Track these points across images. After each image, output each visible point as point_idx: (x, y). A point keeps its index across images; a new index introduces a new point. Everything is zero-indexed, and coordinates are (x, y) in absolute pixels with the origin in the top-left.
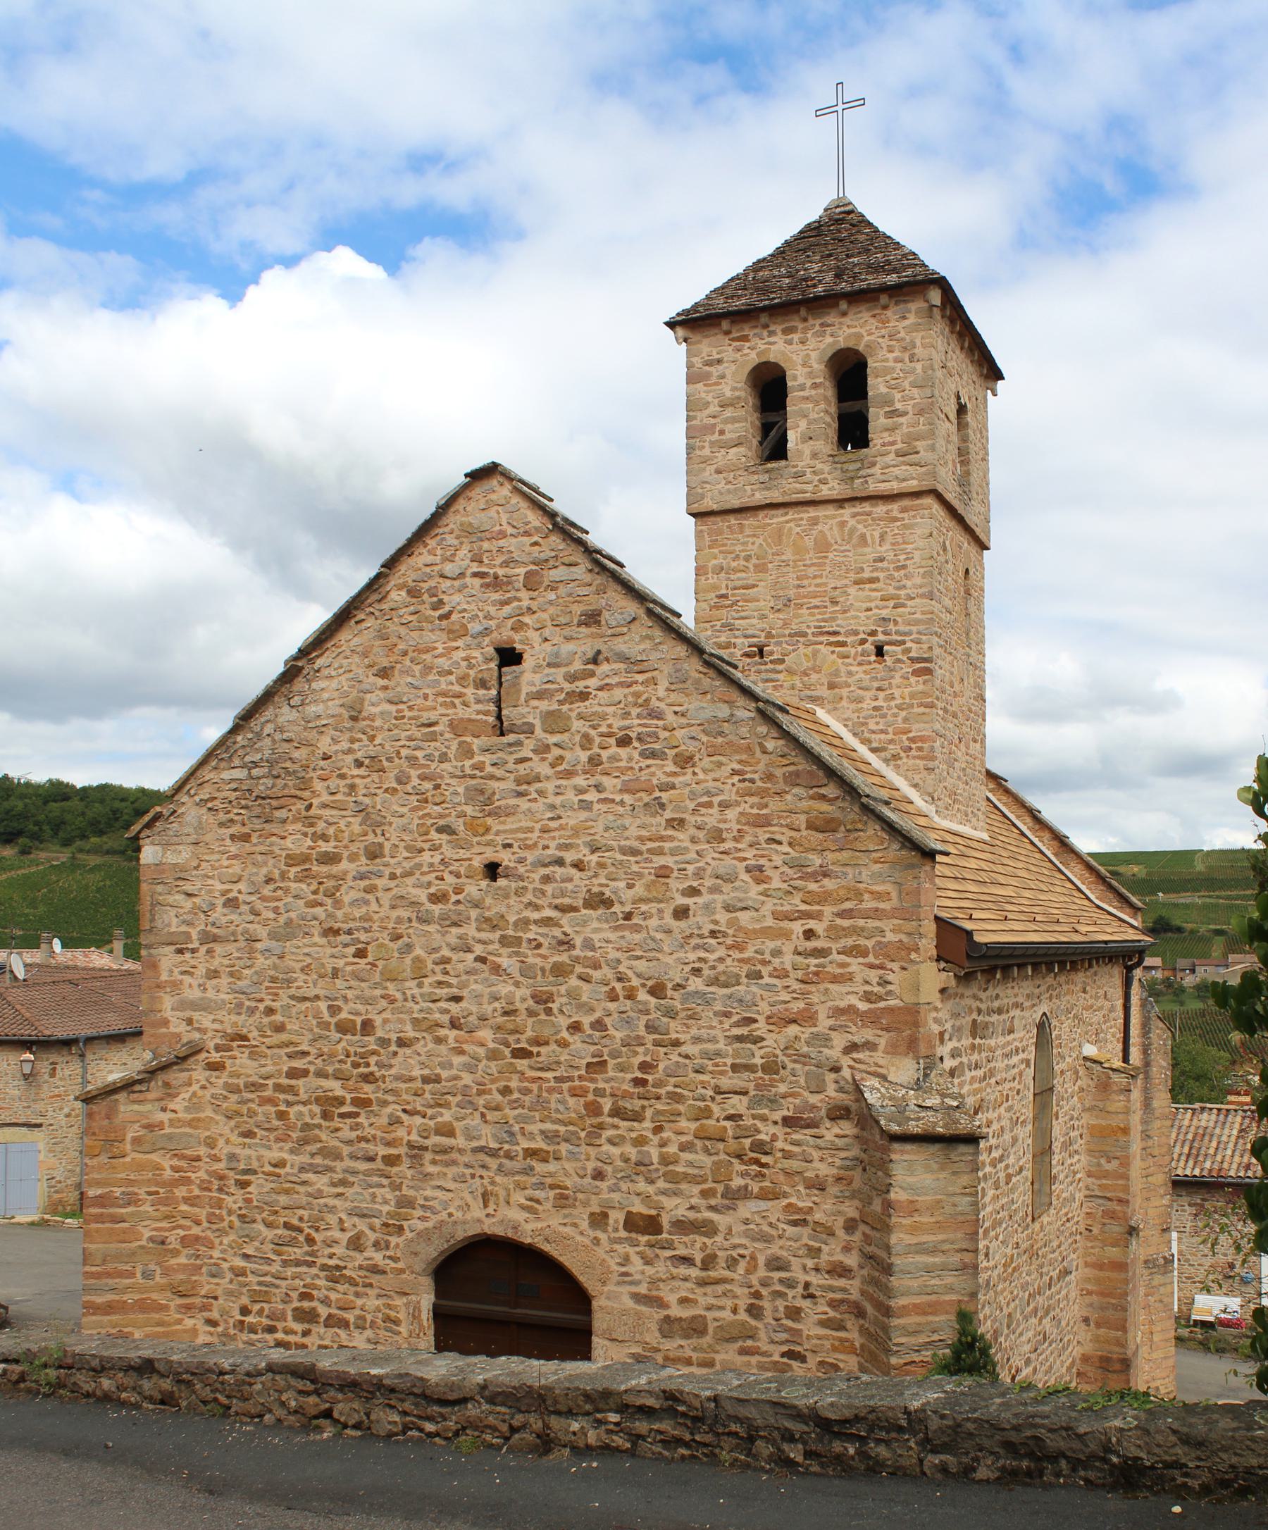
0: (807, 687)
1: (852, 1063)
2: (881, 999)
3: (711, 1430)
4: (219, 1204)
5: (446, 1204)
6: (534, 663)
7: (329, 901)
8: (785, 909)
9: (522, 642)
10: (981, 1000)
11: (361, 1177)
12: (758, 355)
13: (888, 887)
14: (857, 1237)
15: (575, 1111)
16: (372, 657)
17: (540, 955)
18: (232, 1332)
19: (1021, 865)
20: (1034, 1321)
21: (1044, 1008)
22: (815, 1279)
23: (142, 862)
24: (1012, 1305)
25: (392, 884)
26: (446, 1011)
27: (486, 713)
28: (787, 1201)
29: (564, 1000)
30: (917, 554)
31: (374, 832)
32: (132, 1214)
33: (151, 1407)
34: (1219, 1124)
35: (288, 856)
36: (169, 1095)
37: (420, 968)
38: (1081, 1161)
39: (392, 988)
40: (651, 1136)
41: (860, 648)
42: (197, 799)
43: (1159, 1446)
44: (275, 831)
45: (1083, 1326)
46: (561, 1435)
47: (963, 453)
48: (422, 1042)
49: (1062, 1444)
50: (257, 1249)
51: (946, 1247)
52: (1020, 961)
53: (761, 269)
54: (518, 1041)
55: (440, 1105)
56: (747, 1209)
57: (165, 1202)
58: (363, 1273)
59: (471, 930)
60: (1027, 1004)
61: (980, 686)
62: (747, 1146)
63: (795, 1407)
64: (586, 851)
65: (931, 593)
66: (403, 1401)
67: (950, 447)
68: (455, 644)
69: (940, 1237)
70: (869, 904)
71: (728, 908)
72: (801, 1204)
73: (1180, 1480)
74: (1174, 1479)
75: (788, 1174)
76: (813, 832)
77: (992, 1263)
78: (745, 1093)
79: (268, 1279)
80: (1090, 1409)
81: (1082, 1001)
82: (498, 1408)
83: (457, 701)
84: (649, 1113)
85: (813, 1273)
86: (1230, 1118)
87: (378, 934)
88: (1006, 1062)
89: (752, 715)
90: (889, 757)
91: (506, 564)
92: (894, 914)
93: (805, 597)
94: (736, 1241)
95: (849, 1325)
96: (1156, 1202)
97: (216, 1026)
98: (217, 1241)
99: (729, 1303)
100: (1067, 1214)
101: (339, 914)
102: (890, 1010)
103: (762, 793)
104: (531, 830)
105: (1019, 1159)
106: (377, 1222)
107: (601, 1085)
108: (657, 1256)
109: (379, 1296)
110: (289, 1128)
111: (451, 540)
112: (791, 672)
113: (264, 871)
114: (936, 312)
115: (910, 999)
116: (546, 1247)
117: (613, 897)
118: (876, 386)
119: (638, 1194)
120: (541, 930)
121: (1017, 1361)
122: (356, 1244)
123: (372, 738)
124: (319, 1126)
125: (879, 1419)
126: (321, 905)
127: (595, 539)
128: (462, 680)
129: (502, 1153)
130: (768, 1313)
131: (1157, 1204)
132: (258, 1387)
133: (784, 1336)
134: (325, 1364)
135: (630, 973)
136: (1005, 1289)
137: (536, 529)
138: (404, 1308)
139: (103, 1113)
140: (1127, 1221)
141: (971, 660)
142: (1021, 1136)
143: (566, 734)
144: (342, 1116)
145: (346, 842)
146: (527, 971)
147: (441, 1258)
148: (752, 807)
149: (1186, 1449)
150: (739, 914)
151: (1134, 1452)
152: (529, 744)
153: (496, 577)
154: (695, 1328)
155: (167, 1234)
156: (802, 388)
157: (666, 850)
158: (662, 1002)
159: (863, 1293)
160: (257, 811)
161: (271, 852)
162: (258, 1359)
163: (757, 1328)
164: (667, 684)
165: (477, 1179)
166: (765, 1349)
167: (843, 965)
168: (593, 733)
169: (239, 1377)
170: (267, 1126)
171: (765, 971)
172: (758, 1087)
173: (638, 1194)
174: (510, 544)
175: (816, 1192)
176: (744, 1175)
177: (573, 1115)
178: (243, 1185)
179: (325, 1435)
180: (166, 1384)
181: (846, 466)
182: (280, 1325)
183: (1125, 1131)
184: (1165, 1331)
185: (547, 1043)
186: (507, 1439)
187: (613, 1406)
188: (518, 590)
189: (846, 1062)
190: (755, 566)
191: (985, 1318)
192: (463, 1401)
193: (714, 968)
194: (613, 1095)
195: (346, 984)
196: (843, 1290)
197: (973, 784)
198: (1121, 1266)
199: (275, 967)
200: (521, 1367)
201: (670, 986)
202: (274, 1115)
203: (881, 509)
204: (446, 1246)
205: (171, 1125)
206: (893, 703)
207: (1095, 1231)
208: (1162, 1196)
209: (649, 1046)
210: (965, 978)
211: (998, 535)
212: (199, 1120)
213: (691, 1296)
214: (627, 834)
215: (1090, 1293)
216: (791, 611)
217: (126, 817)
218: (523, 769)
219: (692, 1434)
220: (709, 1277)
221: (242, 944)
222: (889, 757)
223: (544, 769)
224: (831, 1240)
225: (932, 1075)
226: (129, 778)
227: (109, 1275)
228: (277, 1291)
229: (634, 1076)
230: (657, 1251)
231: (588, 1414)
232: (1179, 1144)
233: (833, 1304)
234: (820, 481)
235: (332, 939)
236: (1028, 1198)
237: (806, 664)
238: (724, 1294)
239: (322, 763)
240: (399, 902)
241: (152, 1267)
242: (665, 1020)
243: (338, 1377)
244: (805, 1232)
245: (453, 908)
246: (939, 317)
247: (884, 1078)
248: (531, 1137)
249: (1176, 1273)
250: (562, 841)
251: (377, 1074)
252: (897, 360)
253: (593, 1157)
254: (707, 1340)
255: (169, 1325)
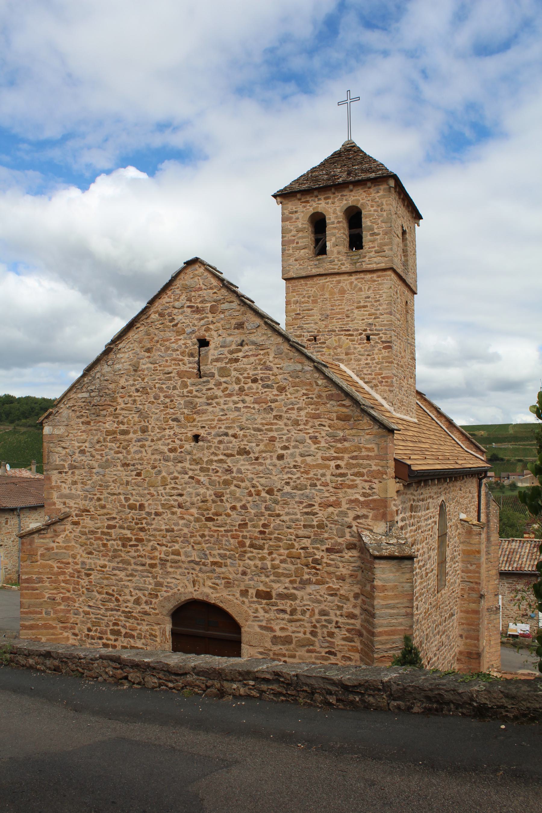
0: (336, 354)
1: (357, 524)
2: (370, 495)
3: (295, 689)
4: (78, 583)
5: (176, 586)
6: (214, 346)
7: (125, 451)
8: (327, 455)
9: (209, 337)
10: (415, 495)
11: (140, 573)
12: (313, 209)
13: (373, 446)
14: (359, 601)
15: (234, 545)
16: (143, 343)
17: (218, 476)
18: (84, 639)
19: (432, 433)
20: (438, 637)
21: (443, 498)
22: (340, 620)
23: (44, 433)
24: (428, 630)
25: (152, 444)
26: (175, 500)
27: (193, 368)
28: (328, 585)
29: (228, 496)
30: (384, 295)
31: (144, 421)
32: (41, 587)
33: (50, 672)
34: (520, 547)
35: (107, 431)
36: (56, 535)
37: (165, 481)
38: (459, 566)
39: (152, 490)
40: (267, 556)
41: (359, 337)
42: (67, 406)
43: (495, 698)
44: (101, 420)
45: (460, 638)
46: (228, 690)
47: (405, 251)
48: (166, 514)
49: (451, 697)
50: (94, 603)
51: (399, 605)
52: (432, 478)
53: (314, 171)
54: (208, 514)
55: (174, 542)
56: (310, 589)
57: (55, 582)
58: (140, 615)
59: (187, 465)
60: (435, 496)
61: (413, 353)
62: (310, 561)
63: (332, 680)
64: (238, 430)
65: (391, 312)
66: (159, 673)
67: (399, 249)
68: (179, 337)
69: (396, 601)
70: (364, 453)
71: (302, 455)
72: (334, 587)
73: (504, 713)
74: (501, 713)
75: (329, 573)
76: (340, 421)
77: (419, 612)
78: (309, 538)
79: (99, 616)
80: (464, 681)
81: (459, 494)
82: (201, 678)
83: (180, 363)
84: (266, 546)
85: (340, 617)
86: (525, 545)
87: (146, 466)
88: (426, 522)
89: (312, 369)
90: (373, 385)
91: (202, 302)
92: (376, 457)
93: (334, 314)
94: (305, 603)
95: (356, 640)
96: (492, 583)
97: (76, 506)
98: (77, 599)
99: (302, 630)
100: (453, 589)
101: (129, 457)
102: (374, 501)
103: (317, 404)
104: (213, 420)
105: (432, 565)
106: (146, 593)
107: (245, 534)
108: (270, 609)
109: (147, 625)
110: (108, 551)
111: (178, 292)
112: (329, 348)
113: (96, 438)
114: (392, 190)
115: (383, 496)
116: (221, 605)
117: (250, 450)
118: (366, 222)
119: (262, 582)
120: (218, 465)
121: (430, 655)
122: (137, 602)
123: (143, 379)
124: (121, 550)
125: (370, 685)
126: (121, 453)
127: (241, 290)
128: (183, 353)
129: (201, 563)
130: (320, 634)
131: (493, 583)
132: (96, 665)
133: (327, 644)
134: (125, 655)
135: (258, 484)
136: (425, 623)
137: (216, 286)
138: (158, 630)
139: (28, 543)
140: (479, 592)
141: (409, 342)
142: (433, 555)
143: (229, 377)
144: (131, 546)
145: (132, 425)
146: (212, 483)
147: (175, 609)
148: (312, 410)
149: (507, 700)
150: (307, 458)
151: (484, 701)
152: (213, 382)
153: (198, 308)
154: (287, 640)
155: (55, 596)
156: (333, 223)
157: (274, 429)
158: (272, 497)
159: (362, 626)
160: (93, 411)
161: (99, 430)
162: (96, 653)
163: (314, 641)
164: (273, 355)
165: (190, 575)
166: (318, 650)
167: (353, 481)
168: (241, 377)
169: (88, 661)
170: (98, 550)
171: (318, 483)
172: (315, 535)
173: (262, 582)
174: (204, 293)
175: (341, 581)
176: (309, 573)
177: (233, 547)
178: (88, 575)
179: (125, 687)
180: (56, 662)
181: (353, 257)
182: (104, 636)
183: (479, 552)
184: (496, 639)
185: (221, 515)
186: (205, 691)
187: (251, 678)
188: (207, 313)
189: (354, 524)
190: (312, 300)
191: (416, 636)
192: (185, 674)
193: (295, 482)
194: (250, 538)
195: (132, 488)
196: (353, 624)
197: (410, 397)
198: (477, 612)
199: (101, 480)
200: (211, 660)
201: (276, 490)
202: (101, 545)
203: (368, 276)
204: (177, 604)
205: (57, 549)
206: (374, 362)
207: (465, 596)
208: (495, 580)
209: (266, 516)
210: (407, 486)
211: (420, 288)
212: (69, 546)
213: (285, 627)
214: (256, 422)
215: (463, 624)
216: (329, 321)
217: (37, 411)
218: (209, 393)
219: (286, 691)
220: (293, 618)
221: (87, 470)
222: (373, 385)
223: (219, 393)
224: (348, 603)
225: (393, 529)
226: (38, 394)
227: (31, 613)
228: (103, 622)
229: (259, 530)
230: (270, 607)
231: (240, 681)
232: (502, 556)
233: (348, 631)
234: (341, 264)
235: (126, 468)
236: (435, 583)
237: (335, 344)
238: (300, 626)
239: (121, 390)
240: (155, 452)
241: (49, 610)
242: (273, 505)
243: (130, 662)
244: (336, 599)
245: (179, 455)
246: (393, 192)
247: (371, 531)
248: (214, 556)
249: (501, 613)
250: (227, 425)
251: (146, 528)
252: (375, 211)
253: (241, 565)
254: (293, 646)
255: (57, 635)
